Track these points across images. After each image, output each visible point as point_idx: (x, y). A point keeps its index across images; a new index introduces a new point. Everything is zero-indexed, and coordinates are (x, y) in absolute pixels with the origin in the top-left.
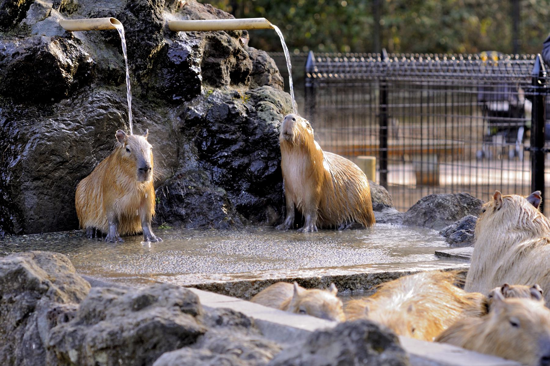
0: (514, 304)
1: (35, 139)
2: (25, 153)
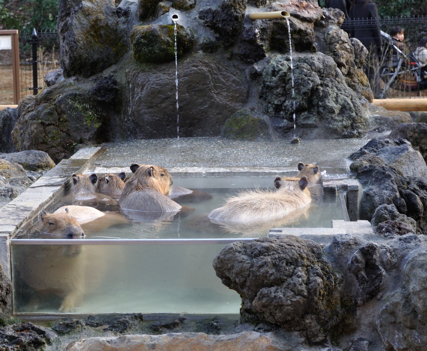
0: (194, 210)
1: (149, 84)
2: (143, 93)
